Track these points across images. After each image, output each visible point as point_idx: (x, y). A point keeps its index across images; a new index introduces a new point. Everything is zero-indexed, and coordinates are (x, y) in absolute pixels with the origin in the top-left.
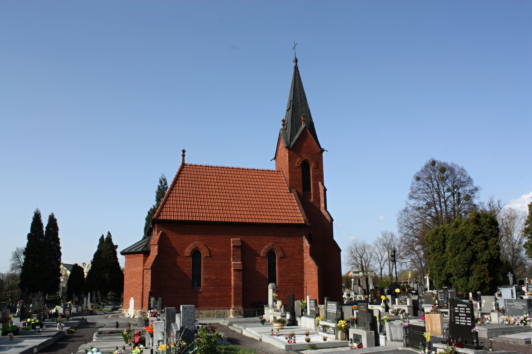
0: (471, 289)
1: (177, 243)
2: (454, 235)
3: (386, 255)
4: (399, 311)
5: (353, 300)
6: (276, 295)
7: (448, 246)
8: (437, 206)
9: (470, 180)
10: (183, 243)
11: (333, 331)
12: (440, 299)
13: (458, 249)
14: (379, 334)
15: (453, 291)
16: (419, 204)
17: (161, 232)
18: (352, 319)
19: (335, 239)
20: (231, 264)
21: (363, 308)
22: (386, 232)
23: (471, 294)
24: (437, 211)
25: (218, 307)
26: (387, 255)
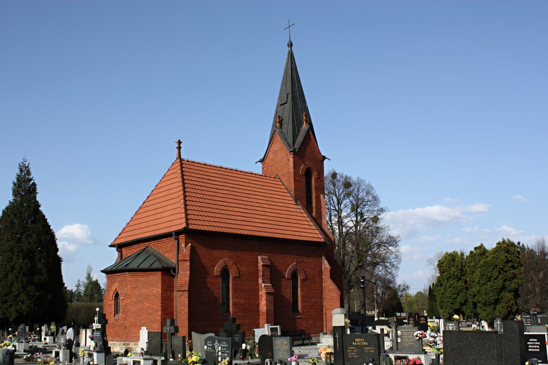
9: (375, 198)
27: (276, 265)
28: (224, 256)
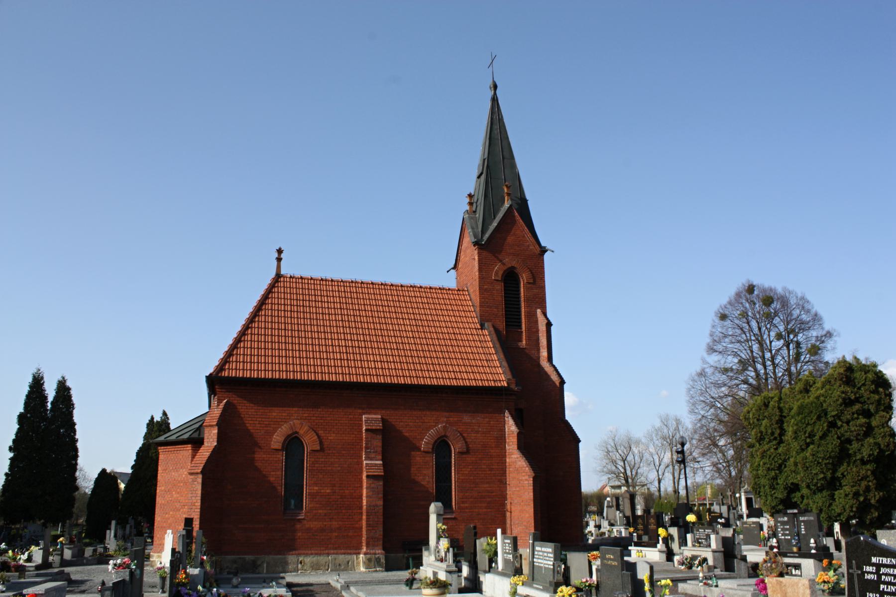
0: (839, 515)
2: (801, 408)
3: (667, 457)
4: (695, 560)
5: (607, 536)
6: (444, 527)
7: (791, 429)
8: (759, 367)
10: (267, 423)
12: (782, 535)
13: (811, 435)
15: (812, 518)
16: (725, 362)
17: (225, 401)
18: (586, 586)
19: (567, 418)
20: (362, 464)
21: (611, 559)
22: (667, 415)
23: (837, 527)
25: (336, 549)
26: (670, 456)
27: (401, 429)
28: (293, 418)
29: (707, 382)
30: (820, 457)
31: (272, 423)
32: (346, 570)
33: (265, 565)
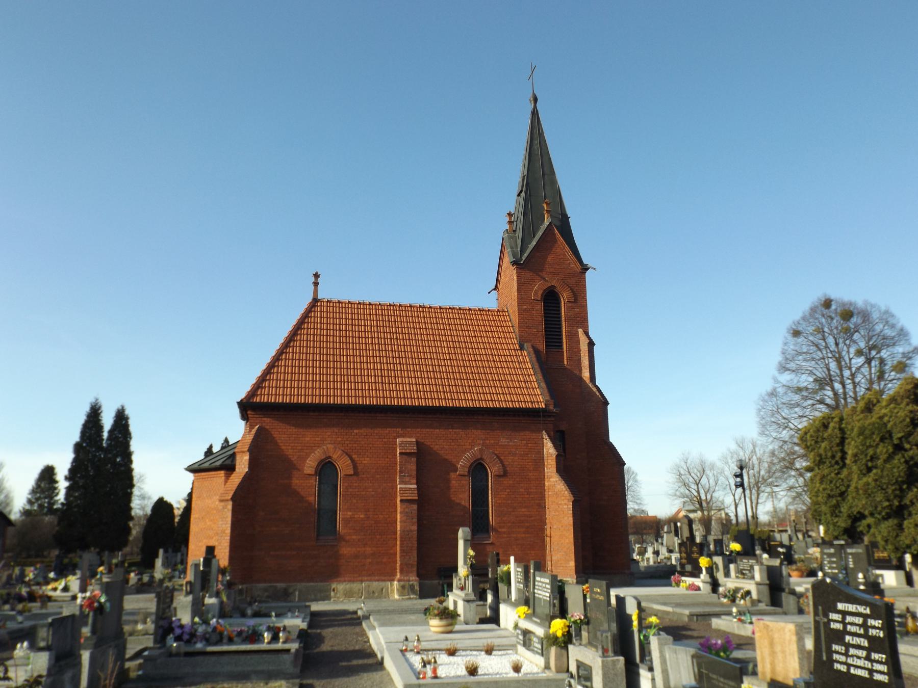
0: (909, 547)
1: (290, 447)
4: (738, 593)
8: (837, 386)
9: (903, 334)
10: (300, 448)
11: (540, 647)
14: (637, 666)
15: (860, 551)
16: (798, 382)
20: (397, 488)
21: (597, 593)
24: (836, 394)
25: (369, 575)
28: (327, 442)
29: (779, 402)
30: (885, 483)
31: (305, 448)
32: (380, 598)
33: (297, 593)
